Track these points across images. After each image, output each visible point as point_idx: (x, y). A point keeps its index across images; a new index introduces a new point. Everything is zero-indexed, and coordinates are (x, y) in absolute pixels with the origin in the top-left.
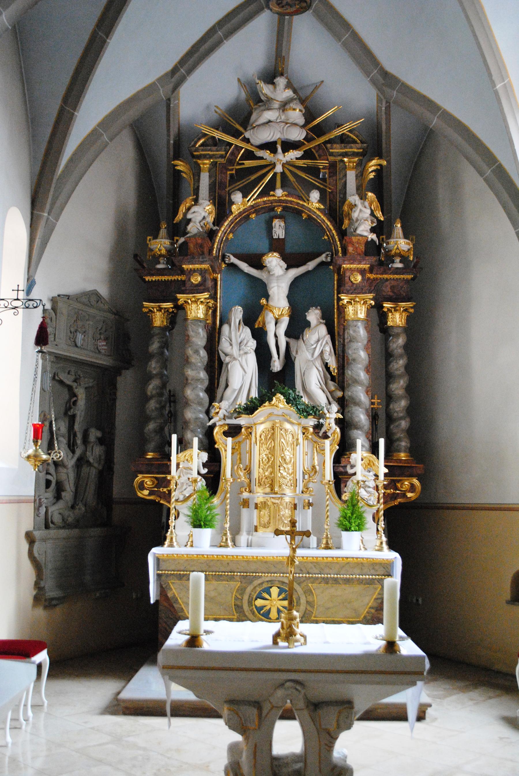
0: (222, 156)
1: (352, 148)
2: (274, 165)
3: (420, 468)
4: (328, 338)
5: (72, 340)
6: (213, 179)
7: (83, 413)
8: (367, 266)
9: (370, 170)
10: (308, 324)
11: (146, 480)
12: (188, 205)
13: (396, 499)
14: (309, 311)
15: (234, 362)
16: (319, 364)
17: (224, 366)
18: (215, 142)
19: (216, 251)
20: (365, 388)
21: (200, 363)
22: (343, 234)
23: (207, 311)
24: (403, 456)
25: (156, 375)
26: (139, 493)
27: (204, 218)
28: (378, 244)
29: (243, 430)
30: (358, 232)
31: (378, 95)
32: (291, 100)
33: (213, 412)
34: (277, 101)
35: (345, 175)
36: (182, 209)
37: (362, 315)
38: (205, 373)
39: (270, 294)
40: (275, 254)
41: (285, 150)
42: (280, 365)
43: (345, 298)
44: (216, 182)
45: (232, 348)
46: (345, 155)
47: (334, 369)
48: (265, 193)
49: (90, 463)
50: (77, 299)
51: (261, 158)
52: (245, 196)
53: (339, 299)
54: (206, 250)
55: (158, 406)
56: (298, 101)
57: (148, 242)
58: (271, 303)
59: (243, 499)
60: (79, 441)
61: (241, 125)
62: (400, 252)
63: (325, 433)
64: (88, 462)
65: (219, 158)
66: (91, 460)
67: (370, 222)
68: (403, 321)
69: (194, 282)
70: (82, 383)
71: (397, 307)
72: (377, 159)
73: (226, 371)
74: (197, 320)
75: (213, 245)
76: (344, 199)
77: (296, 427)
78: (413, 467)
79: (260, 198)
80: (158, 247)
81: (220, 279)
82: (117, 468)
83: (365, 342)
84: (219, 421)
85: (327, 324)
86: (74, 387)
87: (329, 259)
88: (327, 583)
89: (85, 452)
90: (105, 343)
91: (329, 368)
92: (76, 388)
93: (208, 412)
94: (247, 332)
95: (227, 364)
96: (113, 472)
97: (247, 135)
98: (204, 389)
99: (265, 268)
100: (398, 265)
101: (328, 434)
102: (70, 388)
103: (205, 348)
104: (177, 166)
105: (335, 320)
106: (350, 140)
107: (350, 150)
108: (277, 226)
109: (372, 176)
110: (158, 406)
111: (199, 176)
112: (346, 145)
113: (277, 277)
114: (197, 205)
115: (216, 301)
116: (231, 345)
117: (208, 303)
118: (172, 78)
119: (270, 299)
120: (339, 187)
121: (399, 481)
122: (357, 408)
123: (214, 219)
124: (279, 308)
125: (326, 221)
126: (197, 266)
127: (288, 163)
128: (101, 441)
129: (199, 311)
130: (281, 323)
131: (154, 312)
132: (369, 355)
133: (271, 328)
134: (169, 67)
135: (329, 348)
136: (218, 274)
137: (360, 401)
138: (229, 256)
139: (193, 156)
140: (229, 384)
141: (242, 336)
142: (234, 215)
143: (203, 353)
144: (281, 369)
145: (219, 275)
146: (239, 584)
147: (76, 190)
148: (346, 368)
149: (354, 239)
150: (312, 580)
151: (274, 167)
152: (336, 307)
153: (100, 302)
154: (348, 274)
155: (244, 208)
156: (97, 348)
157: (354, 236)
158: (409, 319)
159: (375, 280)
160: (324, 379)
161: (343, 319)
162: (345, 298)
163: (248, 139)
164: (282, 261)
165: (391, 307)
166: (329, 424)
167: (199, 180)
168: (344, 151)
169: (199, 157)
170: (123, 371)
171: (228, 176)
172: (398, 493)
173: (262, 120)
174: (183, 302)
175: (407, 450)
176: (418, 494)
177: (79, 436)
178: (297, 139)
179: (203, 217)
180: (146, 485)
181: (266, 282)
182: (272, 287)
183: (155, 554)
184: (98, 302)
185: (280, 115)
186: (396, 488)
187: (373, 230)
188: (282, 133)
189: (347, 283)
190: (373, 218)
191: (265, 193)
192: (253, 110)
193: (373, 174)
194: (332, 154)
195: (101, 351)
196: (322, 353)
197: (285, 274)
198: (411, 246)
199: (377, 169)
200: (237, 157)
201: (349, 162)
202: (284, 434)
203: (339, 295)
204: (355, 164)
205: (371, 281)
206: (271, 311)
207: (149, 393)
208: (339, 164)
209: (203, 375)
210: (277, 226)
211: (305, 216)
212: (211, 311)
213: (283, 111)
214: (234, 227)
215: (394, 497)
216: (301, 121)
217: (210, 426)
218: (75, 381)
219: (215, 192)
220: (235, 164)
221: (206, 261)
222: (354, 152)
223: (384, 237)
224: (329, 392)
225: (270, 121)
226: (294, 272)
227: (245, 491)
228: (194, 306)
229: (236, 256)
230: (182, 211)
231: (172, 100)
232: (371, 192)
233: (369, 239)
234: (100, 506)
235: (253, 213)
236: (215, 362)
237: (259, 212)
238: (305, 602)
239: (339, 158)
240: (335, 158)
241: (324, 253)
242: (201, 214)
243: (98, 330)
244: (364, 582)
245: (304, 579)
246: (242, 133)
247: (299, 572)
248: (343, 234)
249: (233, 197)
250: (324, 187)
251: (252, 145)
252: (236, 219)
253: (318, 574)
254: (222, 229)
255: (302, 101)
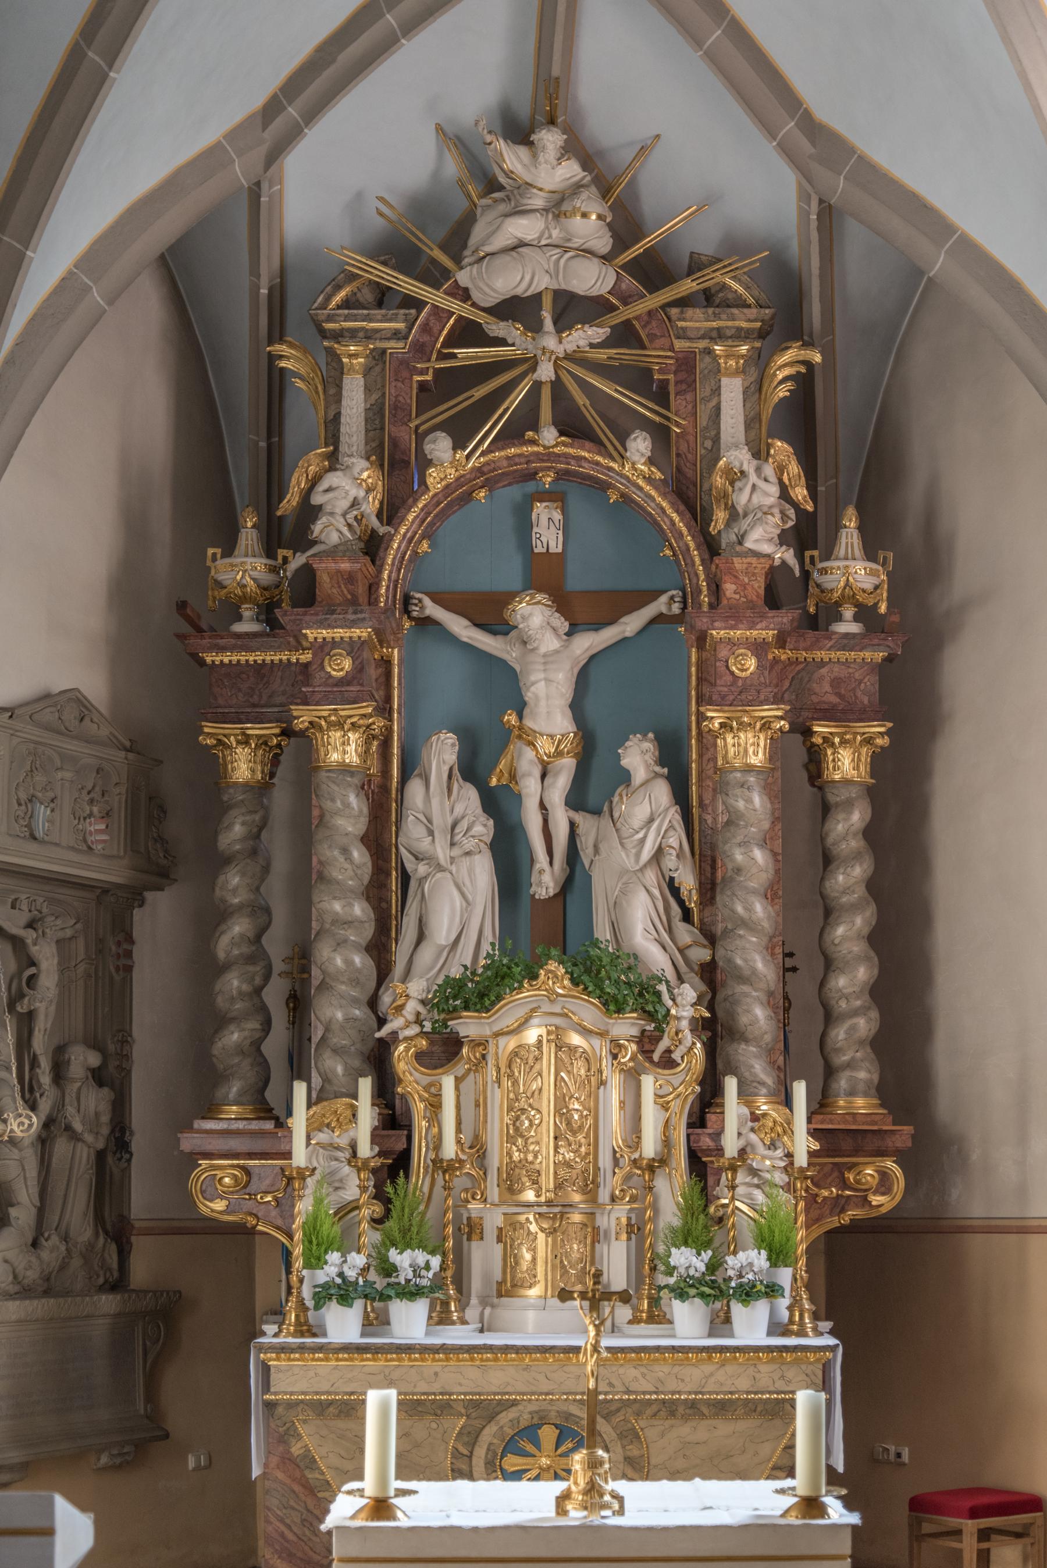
0: (396, 335)
1: (734, 320)
2: (533, 364)
3: (904, 1135)
4: (674, 815)
5: (22, 822)
6: (375, 396)
7: (53, 1008)
8: (770, 634)
9: (780, 375)
10: (625, 777)
11: (219, 1174)
12: (312, 469)
13: (843, 1210)
14: (628, 744)
15: (439, 875)
16: (651, 877)
17: (413, 884)
18: (382, 296)
19: (388, 587)
20: (765, 939)
21: (351, 879)
22: (711, 547)
23: (368, 743)
24: (862, 1104)
25: (241, 907)
26: (201, 1206)
27: (355, 503)
28: (797, 573)
29: (465, 1050)
30: (749, 544)
31: (800, 185)
32: (577, 188)
33: (386, 999)
34: (541, 190)
35: (717, 391)
36: (297, 483)
37: (757, 758)
38: (366, 905)
39: (526, 699)
40: (539, 597)
41: (562, 325)
42: (556, 882)
43: (716, 717)
44: (384, 404)
45: (433, 841)
46: (719, 335)
47: (690, 891)
48: (512, 434)
49: (74, 1131)
50: (30, 717)
51: (502, 342)
52: (459, 444)
53: (701, 717)
54: (361, 590)
55: (245, 987)
56: (593, 189)
57: (209, 563)
58: (528, 723)
59: (469, 1219)
60: (45, 1079)
61: (444, 247)
62: (854, 594)
63: (668, 1051)
64: (68, 1128)
65: (389, 339)
66: (78, 1126)
67: (778, 516)
68: (862, 768)
69: (334, 673)
70: (48, 931)
71: (845, 733)
72: (799, 348)
73: (419, 896)
74: (345, 769)
75: (380, 572)
76: (714, 455)
77: (596, 1042)
78: (886, 1131)
79: (500, 449)
80: (238, 577)
81: (400, 660)
82: (138, 1143)
83: (766, 825)
84: (407, 1026)
85: (669, 778)
86: (29, 941)
87: (676, 608)
88: (672, 1414)
89: (59, 1105)
90: (103, 827)
91: (679, 889)
92: (35, 944)
93: (373, 1003)
94: (469, 798)
95: (422, 881)
96: (131, 1154)
97: (463, 277)
98: (364, 943)
99: (513, 633)
100: (848, 626)
101: (673, 1056)
102: (17, 943)
103: (365, 840)
104: (281, 357)
105: (694, 765)
106: (730, 296)
107: (730, 323)
108: (544, 520)
109: (782, 392)
110: (245, 987)
111: (340, 387)
112: (717, 310)
113: (545, 656)
114: (336, 470)
115: (391, 720)
116: (431, 833)
117: (368, 727)
118: (264, 128)
119: (526, 711)
120: (703, 420)
121: (851, 1167)
122: (745, 988)
123: (381, 503)
124: (552, 736)
125: (669, 511)
126: (339, 633)
127: (568, 357)
128: (98, 1077)
129: (348, 748)
130: (557, 774)
131: (230, 747)
132: (775, 854)
133: (530, 787)
134: (258, 100)
135: (677, 838)
136: (393, 648)
137: (754, 971)
138: (420, 601)
139: (324, 334)
140: (426, 933)
141: (459, 810)
142: (431, 494)
143: (359, 854)
144: (557, 890)
145: (396, 651)
146: (462, 1421)
147: (25, 435)
148: (718, 890)
149: (738, 564)
150: (636, 1406)
151: (533, 369)
152: (694, 733)
153: (87, 720)
154: (723, 653)
155: (457, 474)
156: (85, 840)
157: (739, 555)
158: (878, 761)
159: (792, 662)
160: (664, 918)
161: (711, 764)
162: (716, 717)
163: (466, 290)
164: (557, 615)
165: (831, 733)
166: (677, 1034)
167: (338, 398)
168: (714, 324)
169: (338, 336)
170: (149, 895)
171: (415, 385)
172: (849, 1197)
173: (499, 242)
174: (306, 724)
175: (873, 1091)
176: (898, 1198)
177: (45, 1064)
178: (594, 292)
179: (352, 499)
180: (218, 1186)
181: (518, 668)
182: (533, 684)
183: (427, 1334)
184: (82, 720)
185: (547, 228)
186: (844, 1184)
187: (783, 539)
188: (554, 274)
189: (721, 677)
190: (787, 506)
191: (512, 434)
192: (479, 211)
193: (789, 385)
194: (683, 334)
195: (94, 847)
196: (659, 854)
197: (565, 647)
198: (883, 577)
199: (798, 372)
200: (437, 339)
201: (728, 357)
202: (566, 1060)
203: (702, 709)
204: (742, 361)
205: (780, 666)
206: (531, 744)
207: (221, 955)
208: (701, 360)
209: (359, 909)
210: (544, 520)
211: (613, 497)
212: (375, 743)
213: (557, 217)
214: (432, 524)
215: (839, 1205)
216: (603, 243)
217: (380, 1040)
218: (31, 925)
219: (382, 429)
220: (434, 356)
221: (364, 619)
222: (739, 329)
223: (816, 553)
224: (678, 949)
225: (522, 244)
226: (587, 643)
227: (474, 1198)
228: (336, 735)
229: (438, 599)
230: (299, 483)
231: (265, 186)
232: (780, 439)
233: (777, 563)
234: (101, 1240)
235: (482, 487)
236: (389, 875)
237: (496, 482)
238: (622, 1460)
239: (702, 344)
240: (688, 344)
241: (663, 592)
242: (347, 493)
243: (85, 792)
244: (759, 1409)
245: (619, 1405)
246: (446, 274)
247: (608, 1389)
248: (711, 547)
249: (428, 448)
250: (663, 421)
251: (474, 305)
252: (439, 503)
253: (650, 1393)
254: (402, 531)
255: (605, 193)
